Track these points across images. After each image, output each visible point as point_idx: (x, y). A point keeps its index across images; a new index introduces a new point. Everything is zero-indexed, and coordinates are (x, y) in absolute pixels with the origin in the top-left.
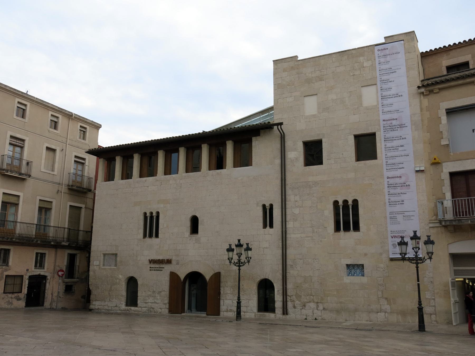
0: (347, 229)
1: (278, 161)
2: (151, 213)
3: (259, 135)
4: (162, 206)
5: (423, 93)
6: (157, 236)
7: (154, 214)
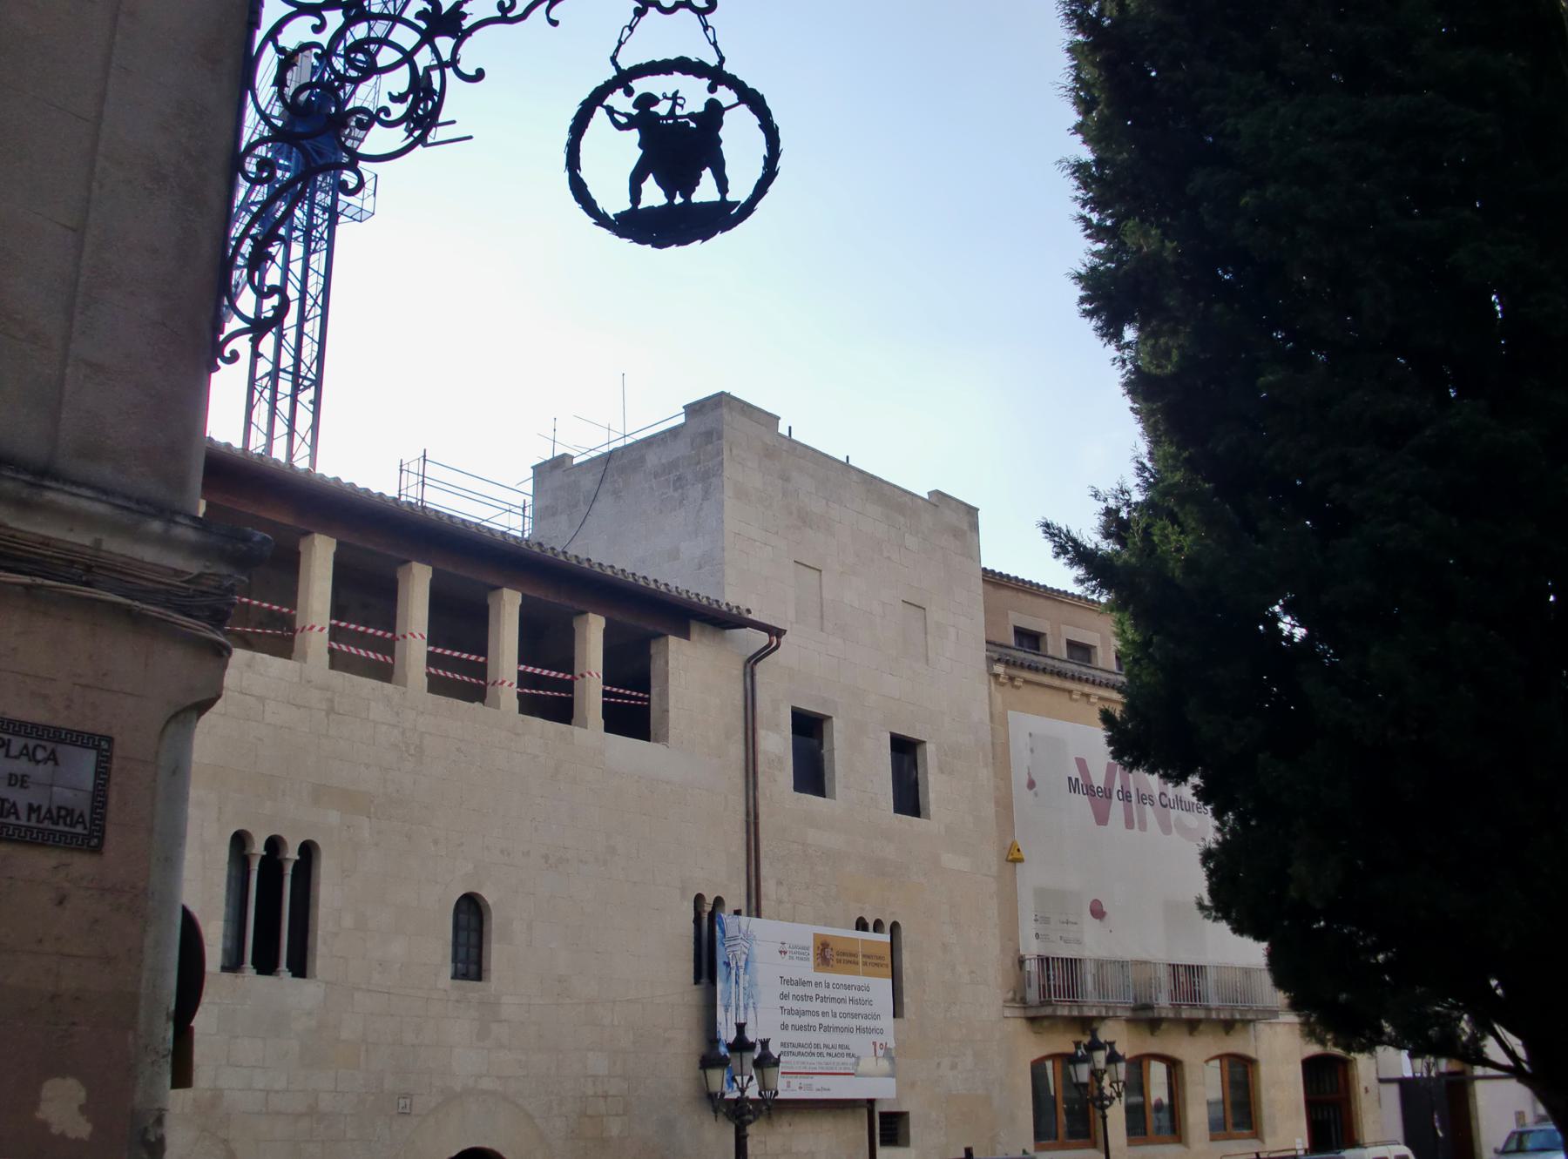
0: (266, 965)
1: (737, 751)
2: (274, 844)
3: (687, 636)
4: (333, 817)
5: (996, 676)
6: (300, 968)
7: (292, 854)
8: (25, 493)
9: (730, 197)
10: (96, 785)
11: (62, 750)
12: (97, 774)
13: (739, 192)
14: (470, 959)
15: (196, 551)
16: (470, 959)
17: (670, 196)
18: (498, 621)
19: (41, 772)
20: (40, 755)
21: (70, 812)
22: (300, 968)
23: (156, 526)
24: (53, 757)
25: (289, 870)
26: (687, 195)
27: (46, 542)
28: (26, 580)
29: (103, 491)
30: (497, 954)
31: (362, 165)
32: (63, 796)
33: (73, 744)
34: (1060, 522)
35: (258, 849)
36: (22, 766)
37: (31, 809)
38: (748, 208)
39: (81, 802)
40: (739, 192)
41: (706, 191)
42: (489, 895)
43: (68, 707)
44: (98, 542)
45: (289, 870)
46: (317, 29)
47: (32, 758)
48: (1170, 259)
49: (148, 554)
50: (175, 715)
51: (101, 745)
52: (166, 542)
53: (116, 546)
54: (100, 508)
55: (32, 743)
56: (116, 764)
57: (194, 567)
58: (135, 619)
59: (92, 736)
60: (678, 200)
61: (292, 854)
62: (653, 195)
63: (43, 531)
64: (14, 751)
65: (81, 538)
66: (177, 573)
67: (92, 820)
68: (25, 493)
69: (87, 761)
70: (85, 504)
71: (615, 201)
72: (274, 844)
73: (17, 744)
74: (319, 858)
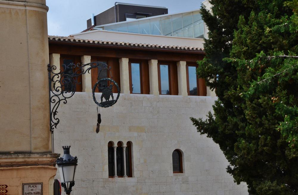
0: (121, 175)
2: (120, 143)
4: (135, 134)
6: (130, 175)
7: (125, 145)
8: (28, 156)
9: (114, 99)
10: (41, 189)
11: (37, 185)
12: (41, 187)
13: (115, 99)
14: (178, 167)
15: (51, 157)
16: (178, 167)
17: (106, 100)
18: (180, 71)
19: (34, 188)
20: (34, 186)
21: (39, 192)
22: (130, 175)
23: (45, 156)
24: (36, 186)
25: (125, 149)
26: (108, 100)
27: (32, 161)
28: (30, 167)
29: (38, 153)
30: (186, 165)
31: (66, 99)
32: (37, 191)
33: (38, 184)
34: (197, 118)
35: (116, 145)
36: (32, 188)
37: (34, 193)
38: (116, 101)
39: (40, 191)
40: (115, 99)
41: (111, 99)
42: (182, 149)
43: (37, 180)
44: (38, 159)
45: (125, 149)
46: (58, 78)
47: (33, 187)
48: (223, 60)
49: (45, 159)
50: (51, 178)
51: (42, 184)
52: (46, 157)
53: (40, 159)
54: (38, 156)
55: (33, 185)
56: (43, 185)
57: (51, 159)
58: (44, 168)
59: (40, 183)
60: (107, 100)
61: (125, 145)
62: (104, 100)
63: (32, 160)
64: (31, 187)
65: (36, 160)
66: (49, 161)
67: (41, 193)
68: (28, 156)
69: (40, 186)
70: (36, 156)
71: (99, 101)
72: (120, 143)
73: (31, 186)
74: (132, 145)
